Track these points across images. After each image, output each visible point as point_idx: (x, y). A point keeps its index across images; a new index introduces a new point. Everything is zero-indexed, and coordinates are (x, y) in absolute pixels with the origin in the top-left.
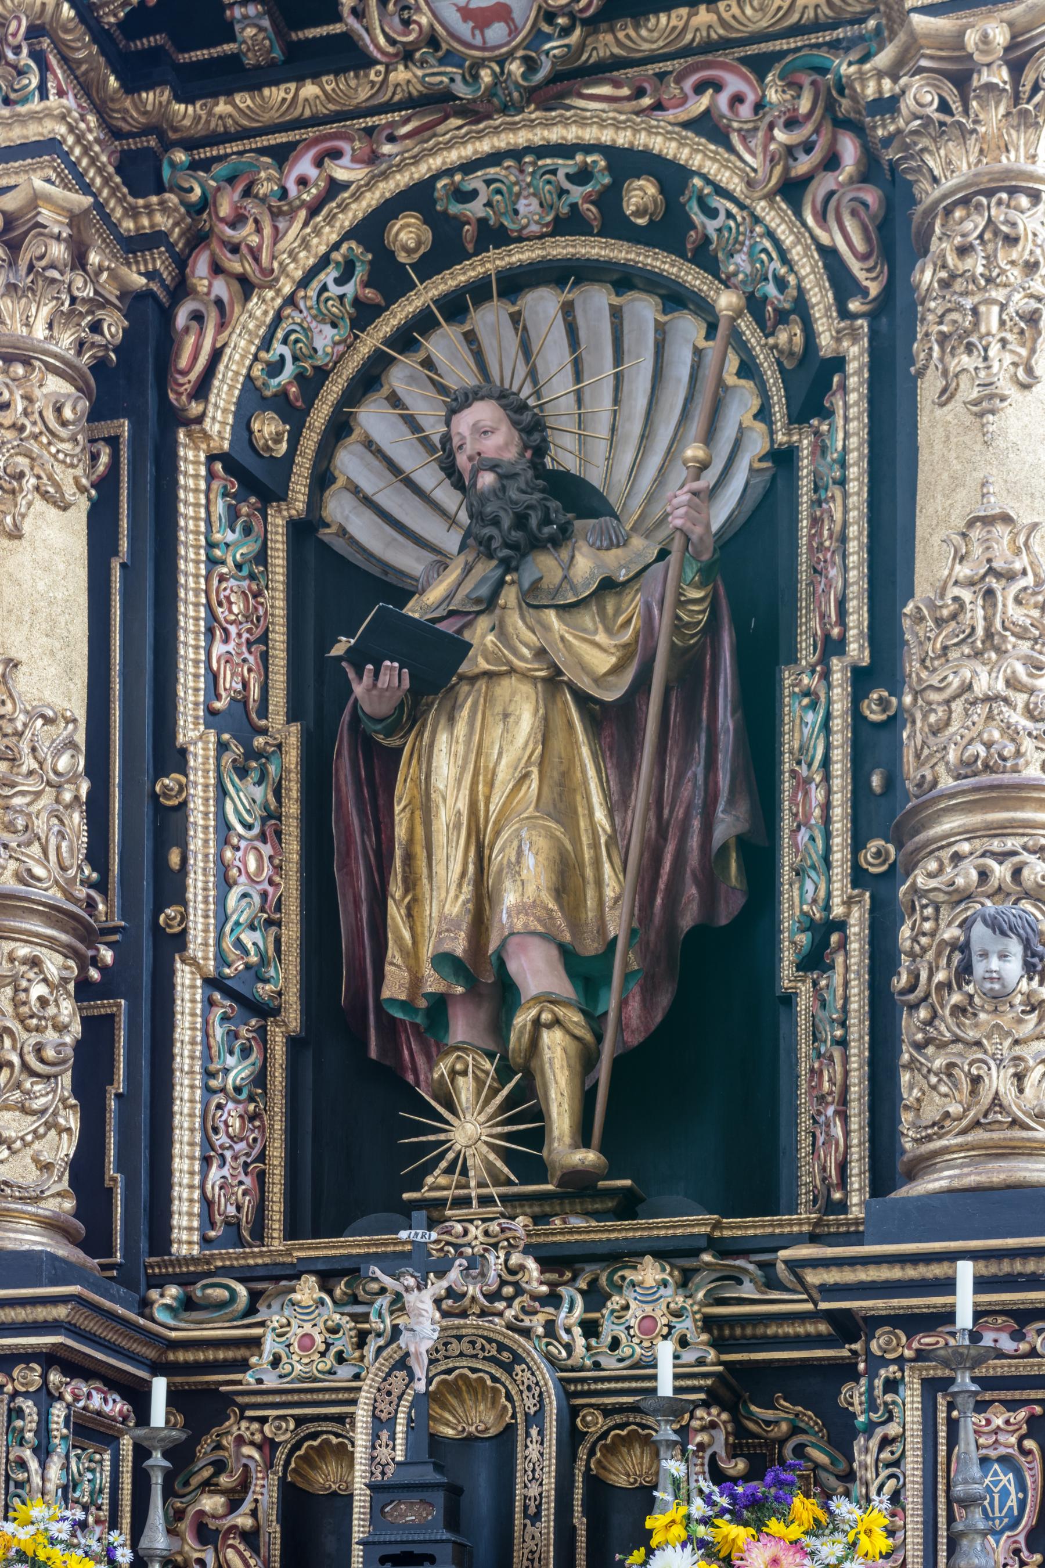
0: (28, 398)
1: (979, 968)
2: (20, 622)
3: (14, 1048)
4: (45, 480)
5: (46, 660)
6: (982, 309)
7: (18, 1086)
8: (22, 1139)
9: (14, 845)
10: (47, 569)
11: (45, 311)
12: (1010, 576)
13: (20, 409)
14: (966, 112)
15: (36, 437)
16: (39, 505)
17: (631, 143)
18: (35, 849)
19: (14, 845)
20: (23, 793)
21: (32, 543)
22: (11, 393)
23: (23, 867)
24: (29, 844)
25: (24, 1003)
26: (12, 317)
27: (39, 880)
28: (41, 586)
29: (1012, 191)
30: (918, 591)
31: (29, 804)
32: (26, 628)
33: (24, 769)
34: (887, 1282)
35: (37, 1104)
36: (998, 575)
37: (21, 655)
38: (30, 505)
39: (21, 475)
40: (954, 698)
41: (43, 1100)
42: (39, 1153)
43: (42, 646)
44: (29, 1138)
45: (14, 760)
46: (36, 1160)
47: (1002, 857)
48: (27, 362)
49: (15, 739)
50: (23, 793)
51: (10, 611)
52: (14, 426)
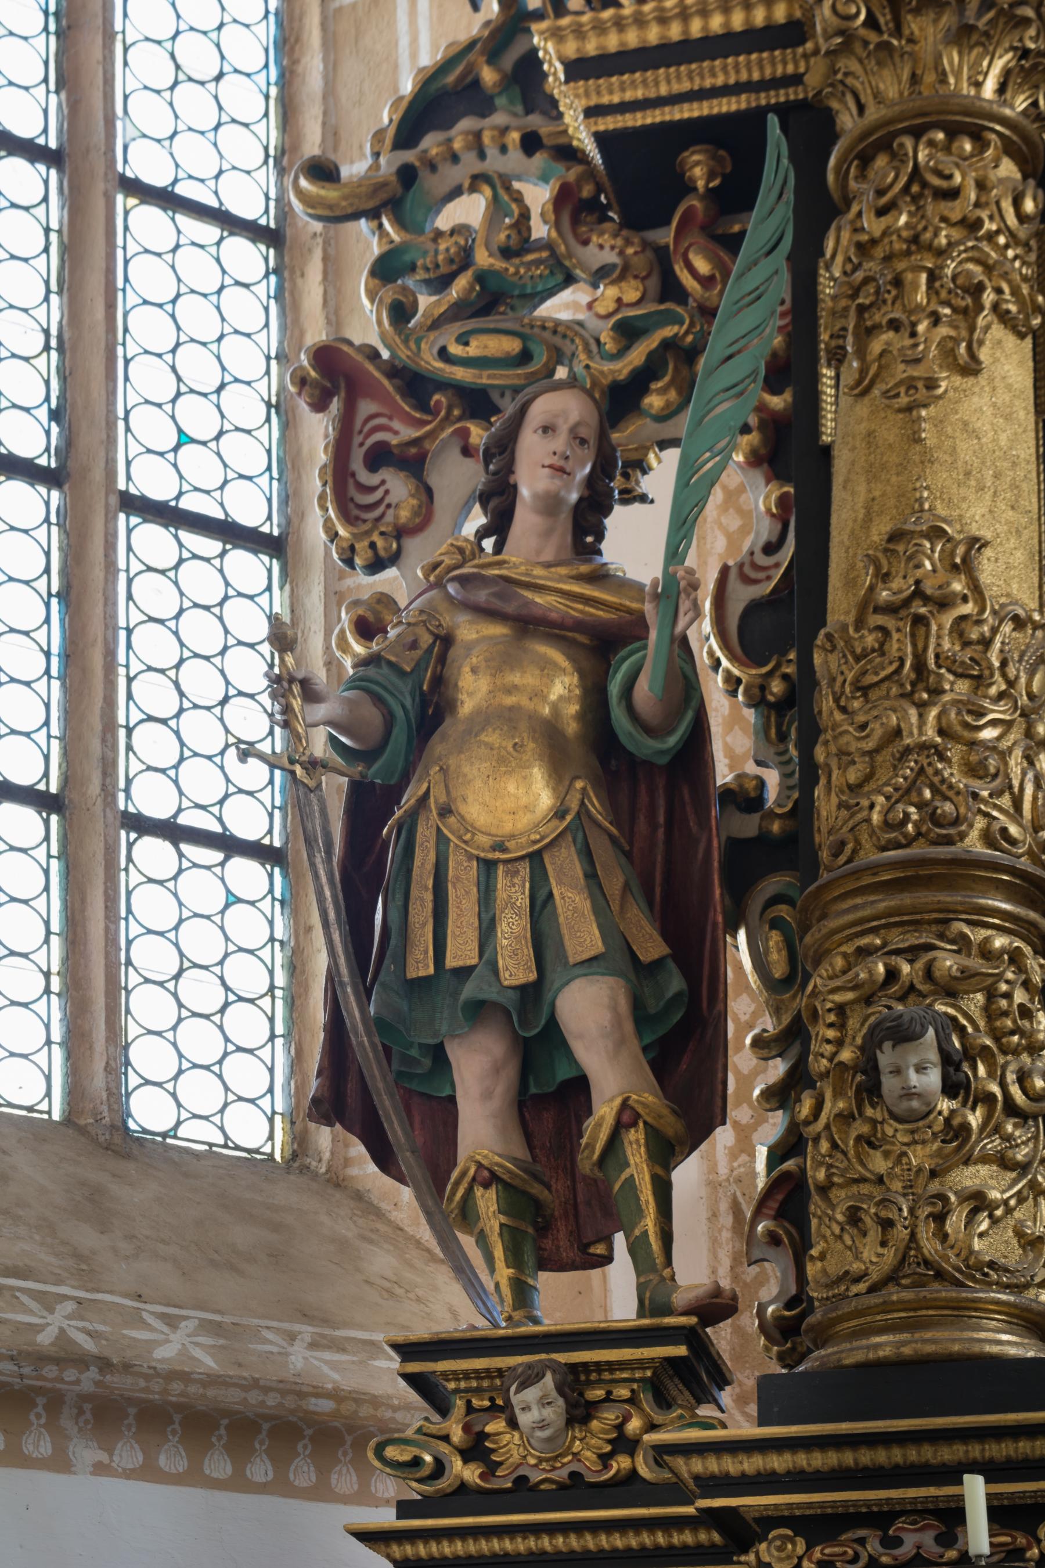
0: (982, 186)
1: (889, 1084)
2: (981, 488)
3: (991, 1074)
4: (1007, 296)
5: (1013, 542)
6: (909, 276)
7: (997, 1129)
8: (1006, 1202)
9: (985, 794)
10: (1008, 418)
11: (999, 65)
12: (943, 604)
13: (973, 196)
14: (898, 32)
15: (991, 237)
16: (998, 331)
17: (622, 44)
18: (1005, 801)
19: (985, 794)
20: (994, 723)
21: (991, 380)
22: (964, 176)
23: (996, 826)
24: (999, 793)
25: (1005, 1014)
26: (958, 75)
27: (1013, 842)
28: (1003, 439)
29: (953, 132)
30: (830, 618)
31: (999, 738)
32: (988, 496)
33: (993, 691)
34: (1009, 1460)
35: (1021, 1155)
36: (926, 599)
37: (987, 534)
38: (987, 328)
39: (980, 288)
40: (877, 750)
41: (1025, 1150)
42: (1021, 1222)
43: (1008, 522)
44: (1012, 1202)
45: (979, 677)
46: (1019, 1234)
47: (912, 953)
48: (977, 136)
49: (980, 648)
50: (994, 723)
51: (968, 474)
52: (963, 222)
